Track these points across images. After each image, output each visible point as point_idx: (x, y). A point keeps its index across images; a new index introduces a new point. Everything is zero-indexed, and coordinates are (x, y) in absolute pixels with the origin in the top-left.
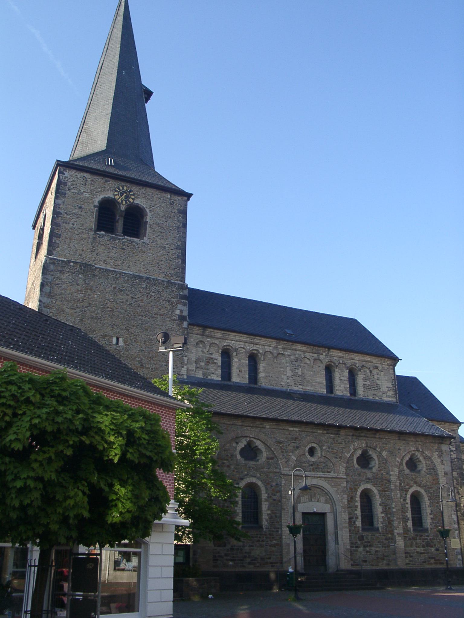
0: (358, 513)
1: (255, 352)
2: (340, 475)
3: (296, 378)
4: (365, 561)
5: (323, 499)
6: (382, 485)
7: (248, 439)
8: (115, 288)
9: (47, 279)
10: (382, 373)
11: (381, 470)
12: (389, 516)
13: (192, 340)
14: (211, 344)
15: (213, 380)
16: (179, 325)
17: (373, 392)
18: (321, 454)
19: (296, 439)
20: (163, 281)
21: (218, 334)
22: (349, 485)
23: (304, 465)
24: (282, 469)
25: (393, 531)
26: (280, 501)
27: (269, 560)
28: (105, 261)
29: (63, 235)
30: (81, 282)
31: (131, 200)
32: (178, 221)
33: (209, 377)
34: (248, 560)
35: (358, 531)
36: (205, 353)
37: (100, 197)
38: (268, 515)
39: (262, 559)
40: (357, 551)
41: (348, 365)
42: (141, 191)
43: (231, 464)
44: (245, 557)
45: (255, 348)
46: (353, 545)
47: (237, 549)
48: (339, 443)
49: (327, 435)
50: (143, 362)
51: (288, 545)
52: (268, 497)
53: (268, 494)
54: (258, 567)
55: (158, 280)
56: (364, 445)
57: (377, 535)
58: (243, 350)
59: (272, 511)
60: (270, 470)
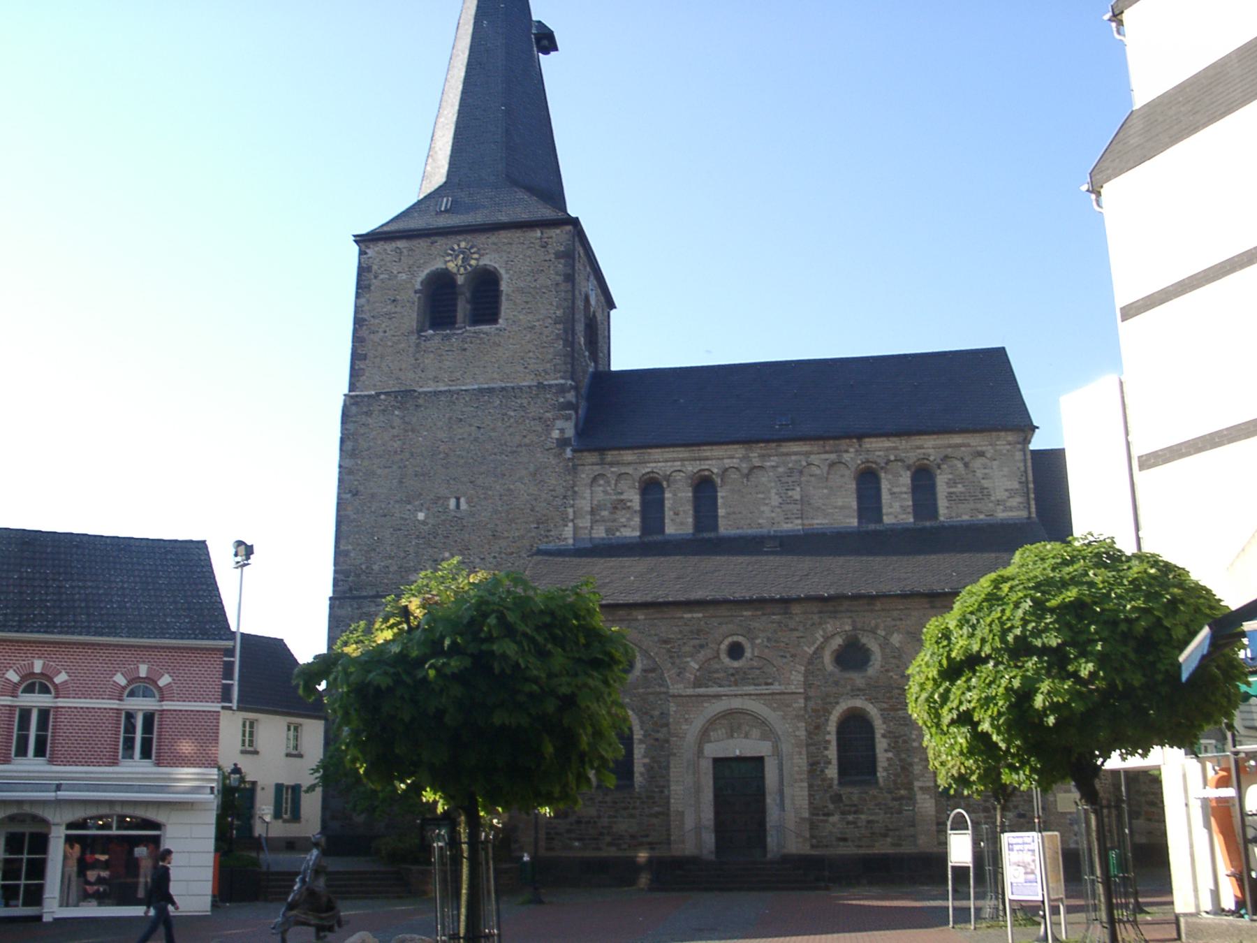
0: (832, 753)
2: (792, 688)
3: (791, 506)
4: (845, 840)
5: (755, 733)
6: (891, 698)
8: (450, 418)
10: (995, 463)
11: (887, 671)
12: (903, 756)
17: (972, 505)
18: (753, 653)
19: (699, 632)
20: (529, 387)
21: (629, 456)
22: (811, 704)
23: (716, 675)
25: (911, 783)
26: (667, 741)
29: (370, 354)
30: (397, 422)
31: (473, 262)
32: (557, 274)
33: (618, 534)
34: (608, 839)
35: (831, 787)
38: (645, 765)
39: (633, 837)
40: (826, 821)
41: (911, 462)
44: (602, 834)
46: (815, 810)
47: (589, 822)
48: (792, 630)
49: (764, 618)
50: (499, 529)
52: (644, 736)
55: (520, 388)
56: (847, 628)
57: (873, 792)
59: (652, 758)
60: (650, 690)
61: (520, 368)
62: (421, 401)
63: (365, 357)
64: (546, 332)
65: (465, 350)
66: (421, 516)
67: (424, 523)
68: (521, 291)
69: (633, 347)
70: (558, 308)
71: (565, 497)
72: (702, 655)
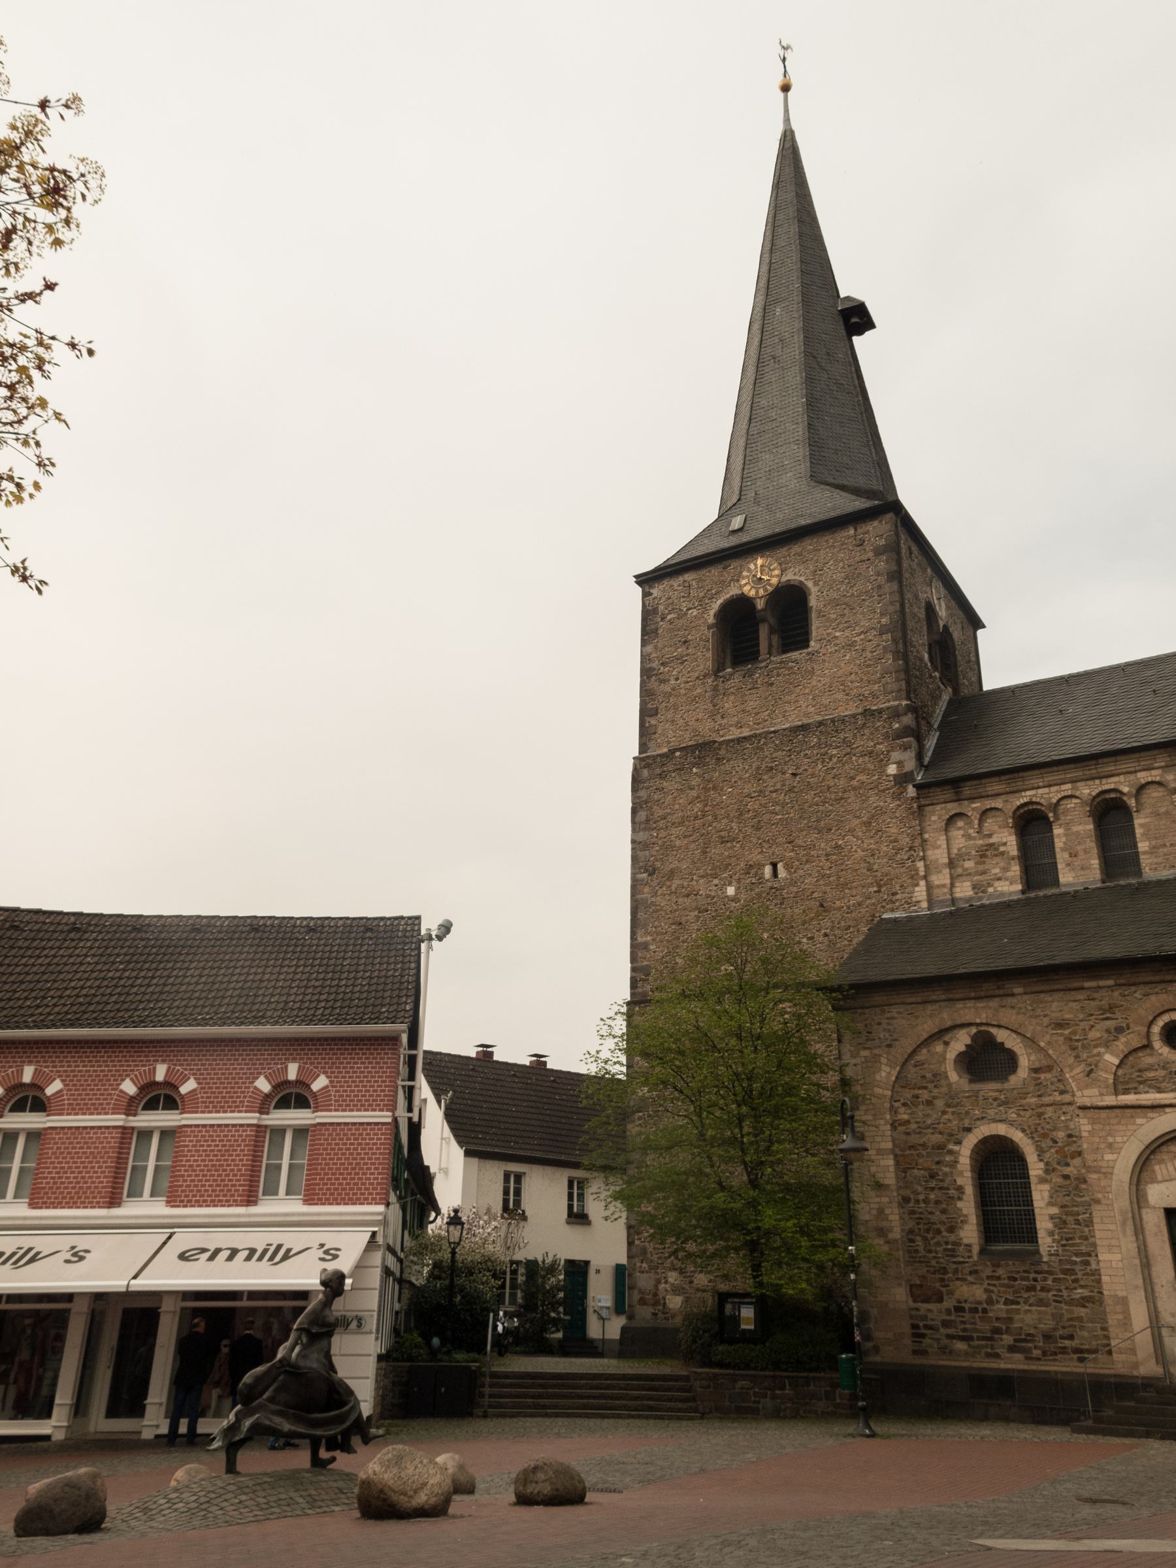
1: (1113, 795)
7: (974, 1030)
8: (758, 768)
9: (639, 797)
13: (933, 818)
14: (985, 813)
15: (1002, 894)
16: (898, 796)
23: (1152, 1074)
24: (1078, 1094)
27: (1067, 1343)
28: (738, 723)
30: (695, 781)
34: (1008, 1339)
36: (974, 839)
37: (716, 605)
38: (1052, 1217)
39: (1047, 1337)
42: (793, 551)
43: (935, 1098)
44: (997, 1331)
45: (1106, 787)
47: (975, 1310)
51: (1124, 1301)
52: (1047, 1171)
53: (1047, 1164)
54: (1039, 1359)
55: (843, 720)
58: (1075, 801)
61: (840, 696)
62: (722, 752)
63: (655, 713)
64: (870, 646)
65: (772, 684)
66: (731, 891)
67: (735, 899)
68: (835, 603)
69: (1006, 659)
70: (882, 615)
71: (911, 848)
72: (1123, 1043)
